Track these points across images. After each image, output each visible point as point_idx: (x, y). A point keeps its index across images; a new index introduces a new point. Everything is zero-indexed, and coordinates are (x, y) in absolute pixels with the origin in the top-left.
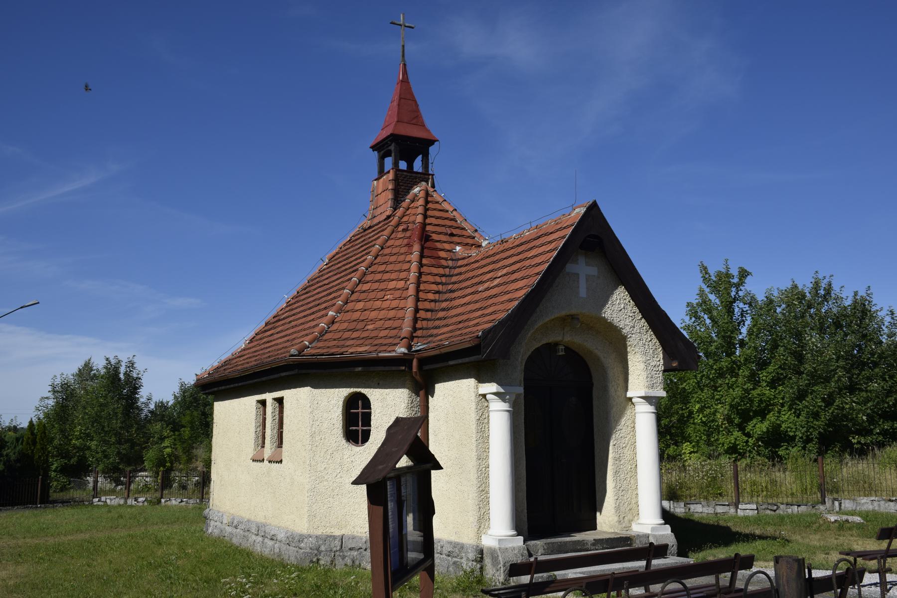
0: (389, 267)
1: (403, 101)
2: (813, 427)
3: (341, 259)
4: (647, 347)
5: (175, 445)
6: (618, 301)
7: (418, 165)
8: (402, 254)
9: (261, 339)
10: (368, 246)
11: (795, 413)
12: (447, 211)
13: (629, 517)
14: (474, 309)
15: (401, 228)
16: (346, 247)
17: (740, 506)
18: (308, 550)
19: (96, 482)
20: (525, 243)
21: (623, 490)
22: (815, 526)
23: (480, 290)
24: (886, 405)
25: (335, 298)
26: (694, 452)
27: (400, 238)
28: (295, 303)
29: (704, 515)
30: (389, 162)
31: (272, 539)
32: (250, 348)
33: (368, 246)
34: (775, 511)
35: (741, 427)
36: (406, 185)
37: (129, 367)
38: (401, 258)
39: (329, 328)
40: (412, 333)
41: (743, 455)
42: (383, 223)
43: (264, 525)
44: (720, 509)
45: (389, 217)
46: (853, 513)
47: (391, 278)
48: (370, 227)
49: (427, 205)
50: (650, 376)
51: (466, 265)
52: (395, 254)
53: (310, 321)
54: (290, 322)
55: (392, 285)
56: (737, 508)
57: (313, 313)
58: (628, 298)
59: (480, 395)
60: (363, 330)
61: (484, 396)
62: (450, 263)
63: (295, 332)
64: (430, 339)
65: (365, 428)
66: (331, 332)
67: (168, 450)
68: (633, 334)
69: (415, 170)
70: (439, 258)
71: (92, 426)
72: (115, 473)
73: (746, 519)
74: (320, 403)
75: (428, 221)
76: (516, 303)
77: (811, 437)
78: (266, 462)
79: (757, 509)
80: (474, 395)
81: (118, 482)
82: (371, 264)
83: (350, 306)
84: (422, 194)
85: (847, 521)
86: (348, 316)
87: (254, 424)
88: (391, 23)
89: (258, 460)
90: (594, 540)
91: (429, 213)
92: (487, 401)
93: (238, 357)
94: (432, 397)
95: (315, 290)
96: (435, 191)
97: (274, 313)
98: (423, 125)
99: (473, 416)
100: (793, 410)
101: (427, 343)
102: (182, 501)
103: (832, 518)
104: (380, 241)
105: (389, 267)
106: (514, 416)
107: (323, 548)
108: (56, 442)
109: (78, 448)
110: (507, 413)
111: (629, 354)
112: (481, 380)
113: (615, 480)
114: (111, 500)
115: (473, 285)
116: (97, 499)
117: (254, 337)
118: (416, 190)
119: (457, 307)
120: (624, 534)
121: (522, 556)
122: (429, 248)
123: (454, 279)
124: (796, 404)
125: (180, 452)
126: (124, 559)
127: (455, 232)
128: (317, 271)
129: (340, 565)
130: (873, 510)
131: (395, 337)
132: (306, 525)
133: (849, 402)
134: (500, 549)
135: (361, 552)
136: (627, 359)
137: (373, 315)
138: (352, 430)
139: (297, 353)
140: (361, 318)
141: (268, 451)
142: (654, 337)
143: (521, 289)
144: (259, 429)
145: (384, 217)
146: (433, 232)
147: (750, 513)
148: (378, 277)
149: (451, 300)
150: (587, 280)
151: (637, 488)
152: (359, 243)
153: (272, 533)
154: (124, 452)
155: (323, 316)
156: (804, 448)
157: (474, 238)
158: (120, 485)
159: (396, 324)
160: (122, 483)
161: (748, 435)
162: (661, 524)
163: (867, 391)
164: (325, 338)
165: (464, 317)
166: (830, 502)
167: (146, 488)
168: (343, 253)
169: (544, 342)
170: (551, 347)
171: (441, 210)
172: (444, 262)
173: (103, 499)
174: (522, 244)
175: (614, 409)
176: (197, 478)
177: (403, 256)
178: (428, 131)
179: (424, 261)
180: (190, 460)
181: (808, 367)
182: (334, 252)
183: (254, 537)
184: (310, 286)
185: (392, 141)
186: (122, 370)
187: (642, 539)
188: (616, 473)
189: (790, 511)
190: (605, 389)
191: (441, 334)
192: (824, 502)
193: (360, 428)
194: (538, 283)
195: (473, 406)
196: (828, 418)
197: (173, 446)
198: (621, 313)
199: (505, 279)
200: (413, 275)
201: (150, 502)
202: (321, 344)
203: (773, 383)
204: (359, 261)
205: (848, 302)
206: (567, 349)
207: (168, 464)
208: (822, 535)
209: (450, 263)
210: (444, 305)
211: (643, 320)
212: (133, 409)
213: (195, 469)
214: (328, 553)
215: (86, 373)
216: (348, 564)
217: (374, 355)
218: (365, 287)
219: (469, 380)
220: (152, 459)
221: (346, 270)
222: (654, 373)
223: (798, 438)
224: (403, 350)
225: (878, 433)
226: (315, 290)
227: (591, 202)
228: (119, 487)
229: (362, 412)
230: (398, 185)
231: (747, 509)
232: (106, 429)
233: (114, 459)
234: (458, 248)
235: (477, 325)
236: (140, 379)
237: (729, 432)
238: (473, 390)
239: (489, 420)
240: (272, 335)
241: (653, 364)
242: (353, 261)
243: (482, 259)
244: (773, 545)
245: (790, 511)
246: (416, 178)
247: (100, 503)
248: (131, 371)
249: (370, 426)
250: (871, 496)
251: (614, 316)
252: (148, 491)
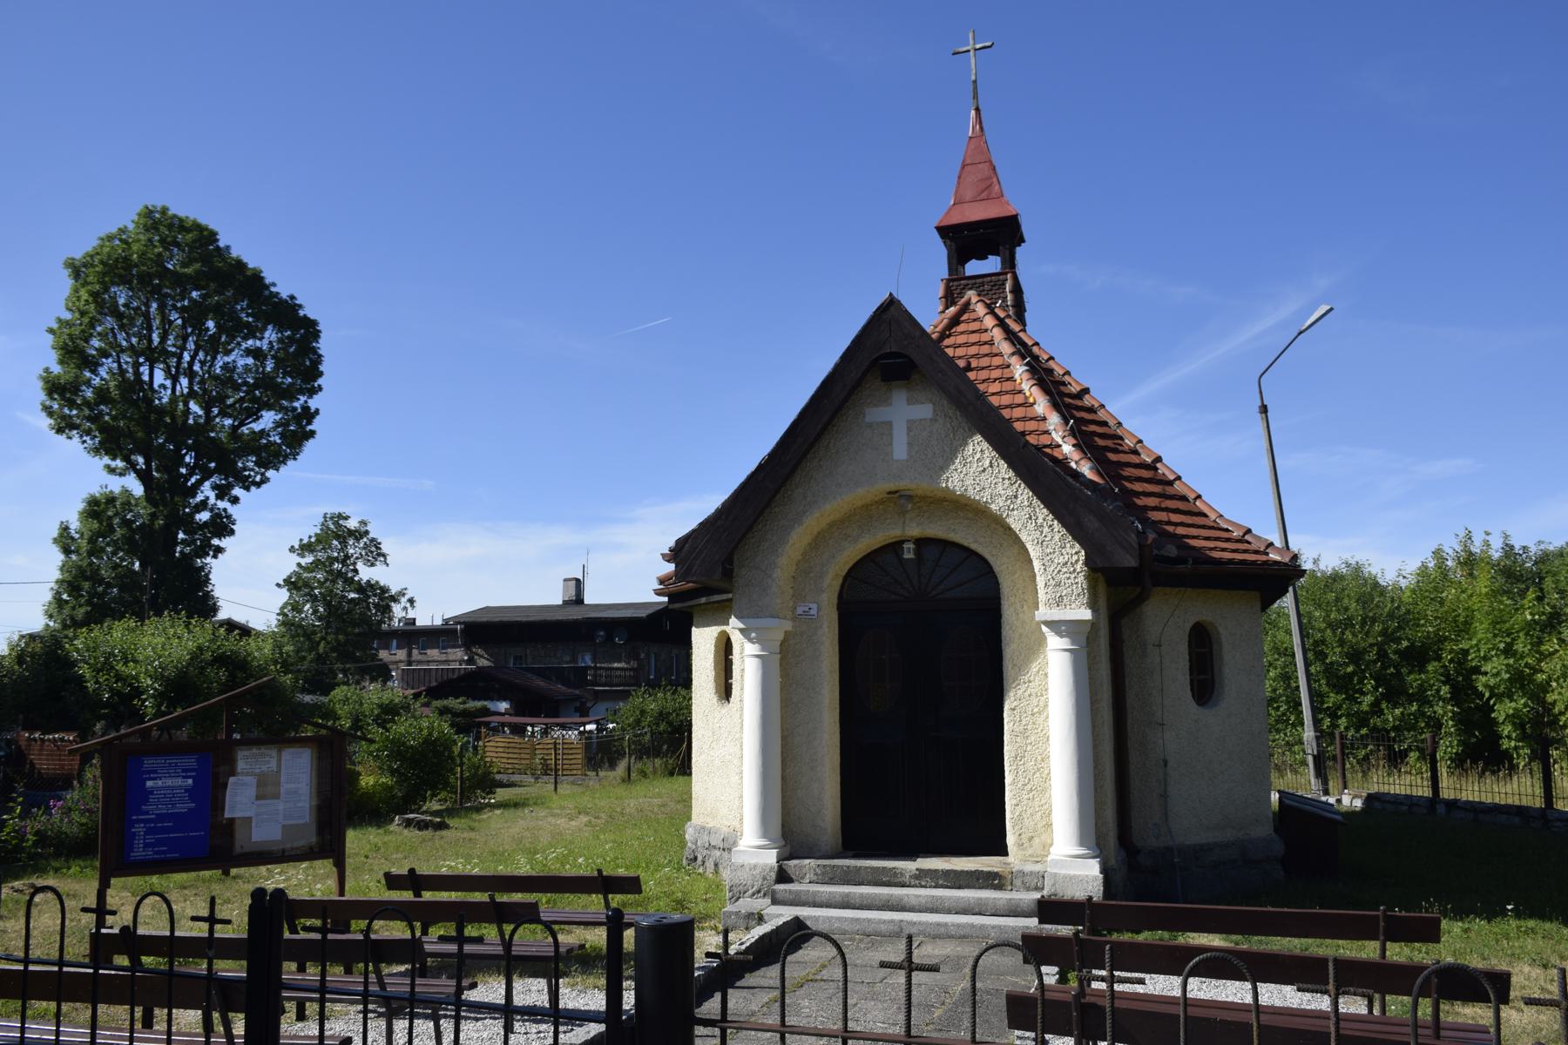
21: (1031, 790)
68: (1013, 510)
88: (954, 54)
90: (917, 869)
110: (1067, 654)
175: (1013, 646)
187: (1027, 879)
251: (968, 483)
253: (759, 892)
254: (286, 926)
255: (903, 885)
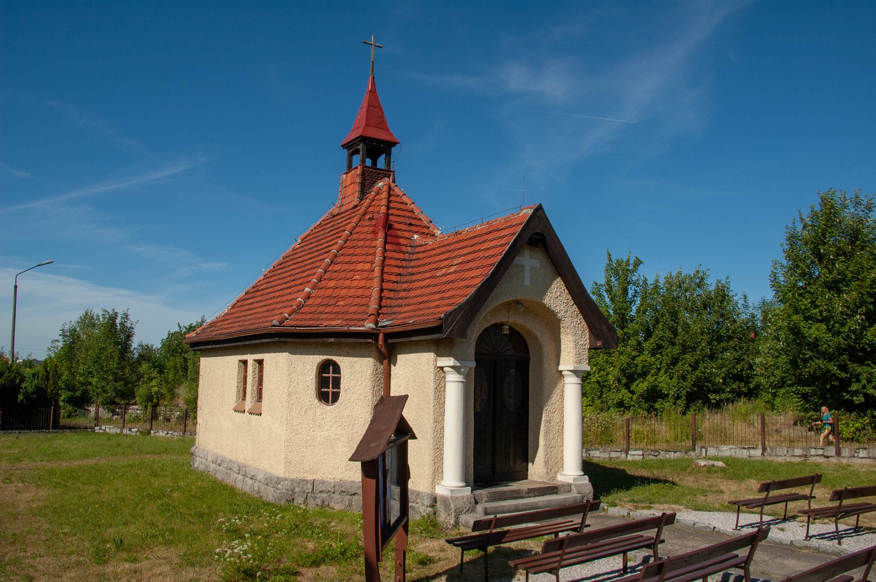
0: (358, 251)
1: (371, 108)
2: (682, 387)
3: (313, 241)
4: (576, 329)
5: (161, 385)
6: (555, 290)
7: (381, 163)
8: (368, 240)
9: (242, 306)
10: (337, 231)
11: (669, 375)
12: (407, 204)
13: (556, 469)
14: (433, 292)
15: (367, 217)
16: (317, 230)
17: (630, 452)
18: (284, 491)
19: (97, 413)
20: (477, 237)
22: (689, 469)
23: (438, 275)
24: (736, 371)
25: (309, 275)
26: (590, 405)
27: (367, 226)
28: (272, 277)
29: (601, 459)
30: (357, 159)
31: (251, 479)
32: (232, 314)
33: (337, 231)
34: (656, 456)
35: (627, 386)
36: (371, 179)
37: (124, 318)
38: (368, 243)
39: (305, 302)
40: (378, 310)
41: (628, 408)
42: (350, 212)
43: (245, 466)
44: (613, 455)
45: (356, 207)
46: (716, 458)
47: (359, 260)
48: (338, 214)
49: (389, 198)
50: (578, 353)
51: (424, 252)
52: (362, 240)
53: (287, 294)
54: (268, 293)
55: (360, 266)
56: (627, 453)
57: (289, 287)
58: (564, 287)
59: (438, 367)
60: (335, 305)
61: (442, 368)
62: (409, 249)
63: (274, 303)
64: (394, 316)
65: (335, 390)
66: (307, 306)
67: (155, 389)
69: (378, 166)
70: (400, 244)
71: (94, 365)
72: (110, 404)
73: (634, 462)
74: (296, 367)
75: (391, 212)
76: (474, 290)
77: (680, 395)
78: (247, 413)
79: (643, 455)
80: (432, 367)
81: (114, 413)
82: (342, 248)
83: (323, 284)
84: (385, 188)
85: (713, 465)
86: (321, 293)
87: (236, 380)
89: (239, 410)
91: (391, 205)
92: (444, 373)
93: (222, 321)
94: (395, 366)
95: (290, 266)
96: (397, 186)
97: (253, 284)
98: (387, 129)
99: (431, 385)
100: (668, 374)
101: (391, 320)
102: (168, 433)
103: (702, 463)
104: (349, 227)
105: (358, 251)
106: (466, 385)
107: (297, 490)
108: (64, 377)
109: (83, 383)
111: (562, 334)
112: (439, 354)
113: (546, 439)
114: (110, 429)
115: (431, 270)
116: (99, 428)
117: (236, 304)
118: (380, 184)
119: (417, 289)
120: (552, 483)
121: (470, 503)
122: (391, 236)
123: (413, 263)
124: (670, 368)
125: (164, 391)
126: (128, 488)
127: (413, 222)
128: (291, 249)
129: (312, 505)
130: (731, 456)
131: (364, 313)
132: (283, 470)
133: (710, 367)
134: (452, 498)
135: (330, 495)
136: (560, 338)
137: (344, 292)
138: (324, 392)
139: (278, 324)
140: (334, 295)
141: (249, 404)
142: (583, 320)
143: (477, 278)
144: (240, 385)
145: (351, 206)
146: (395, 222)
147: (637, 458)
148: (348, 259)
149: (411, 282)
150: (531, 271)
151: (562, 446)
152: (329, 228)
153: (252, 473)
154: (119, 388)
155: (299, 291)
156: (675, 403)
157: (429, 228)
158: (115, 415)
159: (365, 301)
160: (118, 414)
161: (632, 392)
162: (581, 475)
163: (722, 359)
164: (301, 311)
165: (425, 299)
166: (699, 449)
167: (137, 419)
168: (314, 235)
169: (492, 323)
170: (498, 327)
171: (401, 203)
172: (403, 248)
173: (103, 427)
174: (475, 237)
176: (178, 413)
177: (369, 242)
178: (391, 135)
179: (388, 247)
180: (172, 398)
181: (679, 340)
182: (306, 233)
183: (236, 475)
184: (284, 262)
185: (360, 141)
186: (118, 321)
188: (546, 433)
189: (668, 456)
190: (540, 363)
191: (403, 313)
192: (694, 450)
193: (331, 390)
194: (492, 274)
195: (432, 376)
196: (694, 380)
197: (160, 385)
198: (557, 300)
199: (461, 267)
200: (378, 259)
201: (141, 433)
202: (299, 316)
203: (657, 350)
204: (329, 244)
205: (712, 288)
206: (511, 329)
207: (155, 400)
208: (695, 478)
209: (409, 249)
210: (405, 286)
211: (575, 306)
212: (127, 353)
213: (177, 405)
214: (302, 494)
215: (88, 321)
216: (319, 504)
217: (346, 328)
218: (337, 267)
219: (429, 354)
220: (142, 395)
221: (318, 250)
222: (581, 350)
223: (670, 395)
224: (372, 325)
225: (728, 392)
226: (290, 266)
227: (537, 206)
228: (115, 417)
229: (333, 377)
230: (365, 179)
231: (635, 455)
232: (105, 369)
233: (111, 393)
234: (416, 236)
235: (437, 307)
236: (133, 328)
237: (619, 390)
238: (431, 362)
239: (445, 388)
240: (252, 303)
241: (581, 343)
242: (324, 243)
243: (438, 248)
244: (663, 488)
245: (668, 456)
246: (380, 174)
247: (100, 431)
248: (125, 322)
249: (339, 388)
250: (729, 445)
252: (138, 421)
253: (468, 510)
254: (506, 545)
255: (522, 498)
